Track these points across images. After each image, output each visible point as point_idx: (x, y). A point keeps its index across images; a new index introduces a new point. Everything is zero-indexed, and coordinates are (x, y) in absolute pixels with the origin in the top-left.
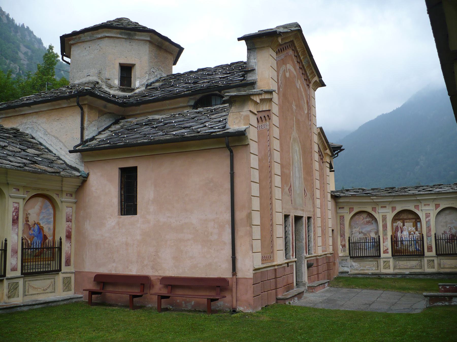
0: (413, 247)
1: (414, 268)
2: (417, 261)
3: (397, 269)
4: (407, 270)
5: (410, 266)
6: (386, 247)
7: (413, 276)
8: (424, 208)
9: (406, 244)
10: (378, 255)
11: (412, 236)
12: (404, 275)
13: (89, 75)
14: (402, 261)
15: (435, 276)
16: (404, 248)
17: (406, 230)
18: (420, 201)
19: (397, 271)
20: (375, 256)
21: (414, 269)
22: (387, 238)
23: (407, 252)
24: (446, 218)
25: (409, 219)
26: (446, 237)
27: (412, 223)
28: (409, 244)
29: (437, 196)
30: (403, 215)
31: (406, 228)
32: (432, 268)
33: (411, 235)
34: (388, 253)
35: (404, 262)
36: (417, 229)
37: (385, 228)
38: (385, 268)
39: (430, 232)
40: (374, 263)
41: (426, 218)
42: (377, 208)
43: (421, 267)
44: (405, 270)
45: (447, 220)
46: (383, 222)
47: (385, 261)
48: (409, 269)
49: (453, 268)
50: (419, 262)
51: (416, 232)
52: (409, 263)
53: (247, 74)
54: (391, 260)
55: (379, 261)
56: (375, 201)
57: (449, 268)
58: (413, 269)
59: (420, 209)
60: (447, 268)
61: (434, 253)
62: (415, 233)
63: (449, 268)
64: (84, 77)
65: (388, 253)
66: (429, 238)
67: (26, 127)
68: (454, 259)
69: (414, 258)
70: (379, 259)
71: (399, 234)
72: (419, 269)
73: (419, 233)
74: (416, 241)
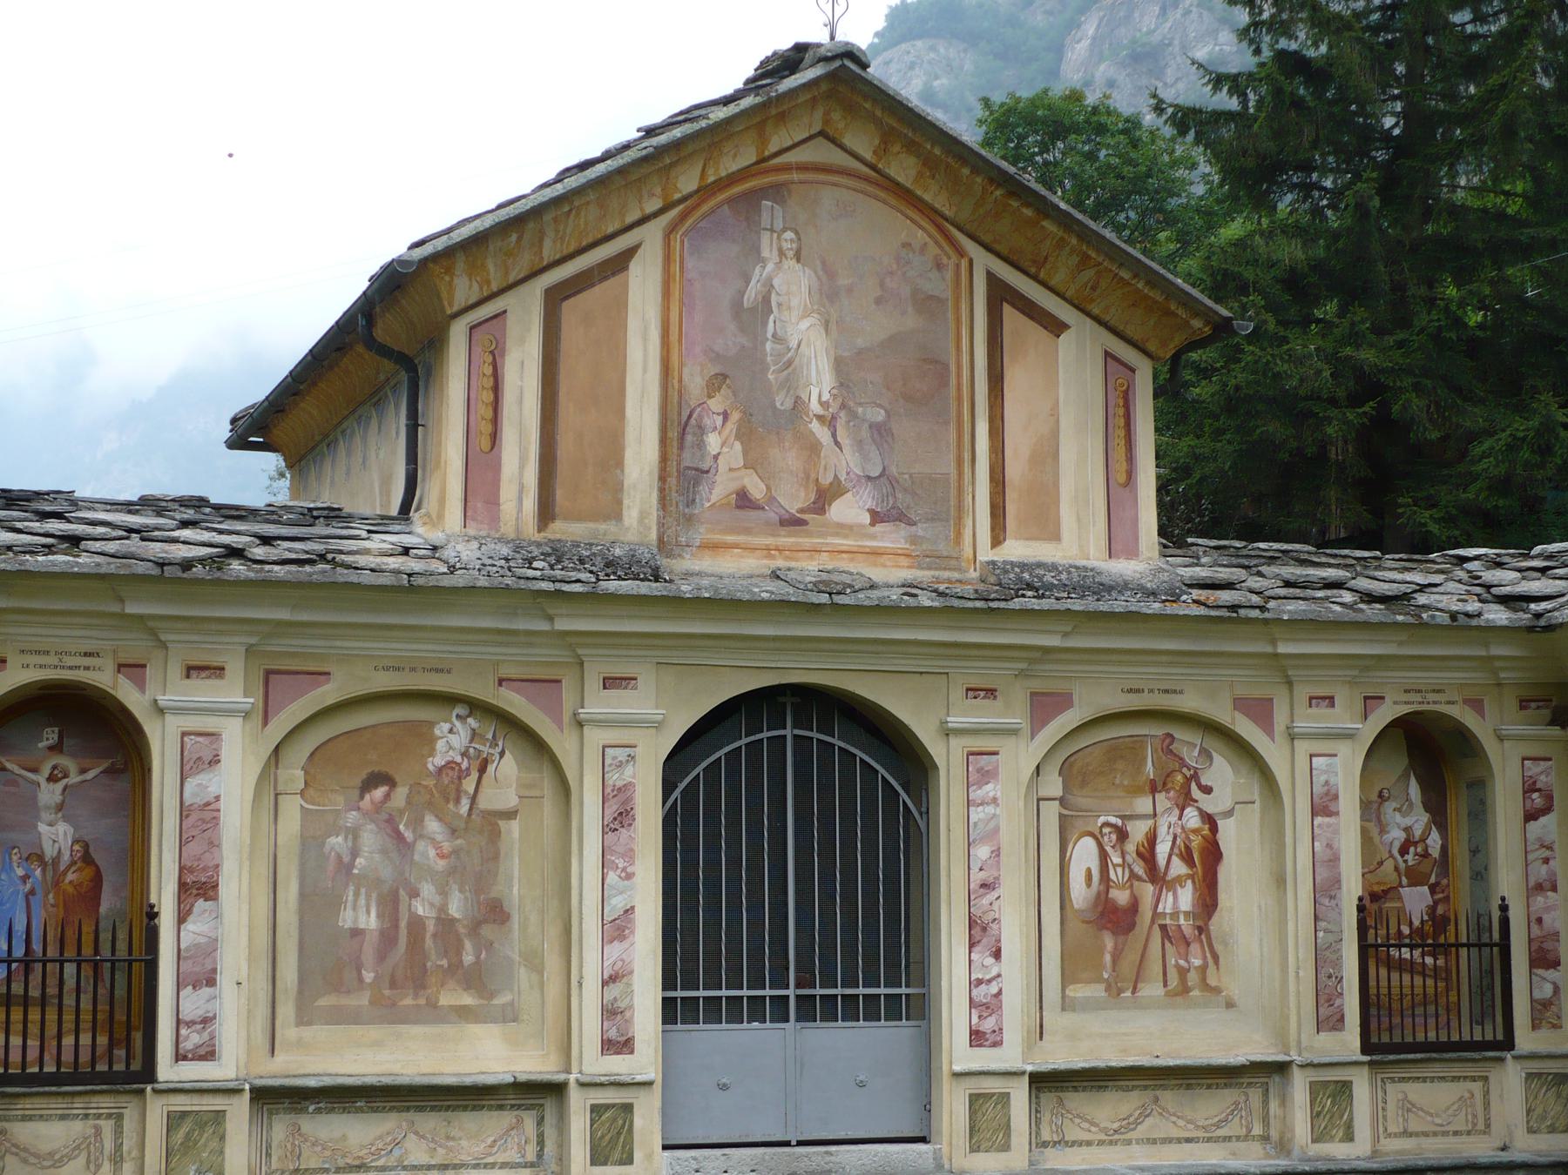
59: (1280, 719)
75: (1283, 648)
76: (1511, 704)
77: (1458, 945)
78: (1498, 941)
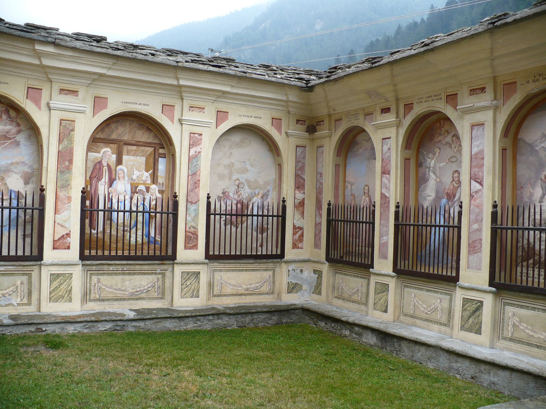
0: (140, 233)
1: (143, 295)
2: (154, 276)
3: (94, 300)
4: (121, 302)
5: (131, 291)
6: (62, 226)
7: (148, 323)
8: (188, 115)
9: (121, 221)
10: (35, 253)
11: (140, 197)
12: (120, 323)
14: (108, 274)
15: (205, 322)
16: (114, 233)
17: (124, 177)
18: (46, 73)
19: (94, 307)
20: (23, 258)
21: (143, 299)
22: (69, 199)
23: (120, 245)
24: (231, 153)
25: (137, 144)
26: (223, 208)
27: (144, 159)
28: (127, 222)
29: (232, 86)
30: (120, 127)
31: (126, 171)
32: (192, 297)
33: (136, 195)
34: (69, 248)
35: (115, 277)
36: (154, 179)
37: (67, 163)
38: (54, 298)
39: (196, 190)
40: (18, 283)
41: (191, 146)
42: (45, 94)
43: (163, 293)
44: (116, 303)
45: (233, 161)
46: (60, 141)
47: (58, 275)
48: (129, 299)
49: (241, 295)
50: (158, 279)
51: (153, 187)
52: (130, 280)
54: (77, 272)
55: (35, 274)
56: (47, 62)
57: (232, 295)
58: (140, 299)
59: (177, 116)
60: (229, 295)
61: (199, 253)
62: (148, 189)
63: (232, 295)
65: (69, 248)
66: (192, 208)
68: (246, 270)
69: (146, 267)
70: (36, 269)
71: (102, 188)
72: (157, 299)
73: (161, 192)
74: (149, 213)
75: (182, 82)
76: (293, 121)
77: (253, 216)
78: (281, 215)
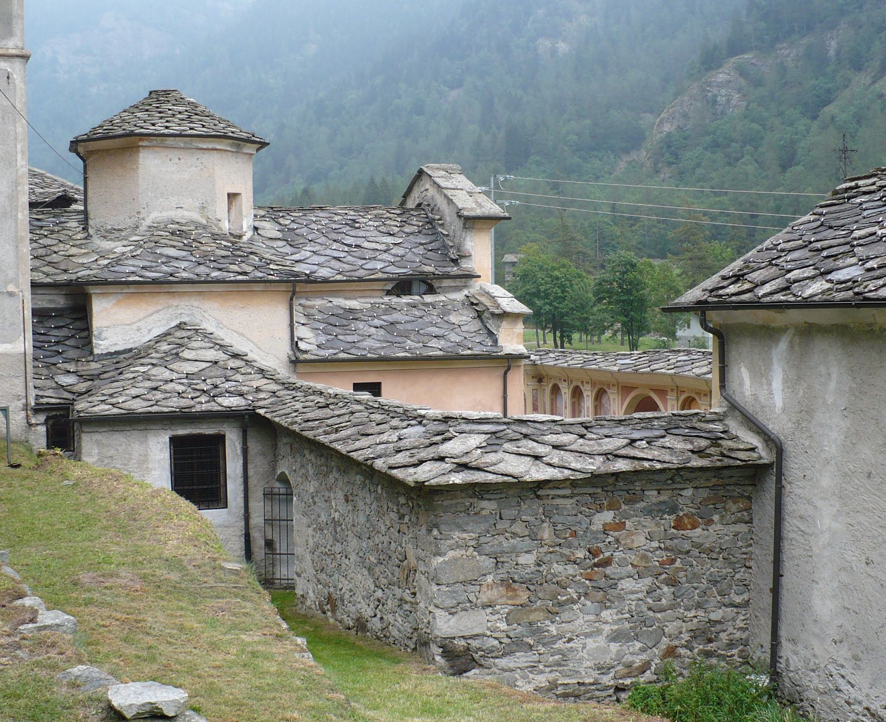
13: (181, 208)
53: (460, 258)
64: (171, 210)
67: (179, 312)
